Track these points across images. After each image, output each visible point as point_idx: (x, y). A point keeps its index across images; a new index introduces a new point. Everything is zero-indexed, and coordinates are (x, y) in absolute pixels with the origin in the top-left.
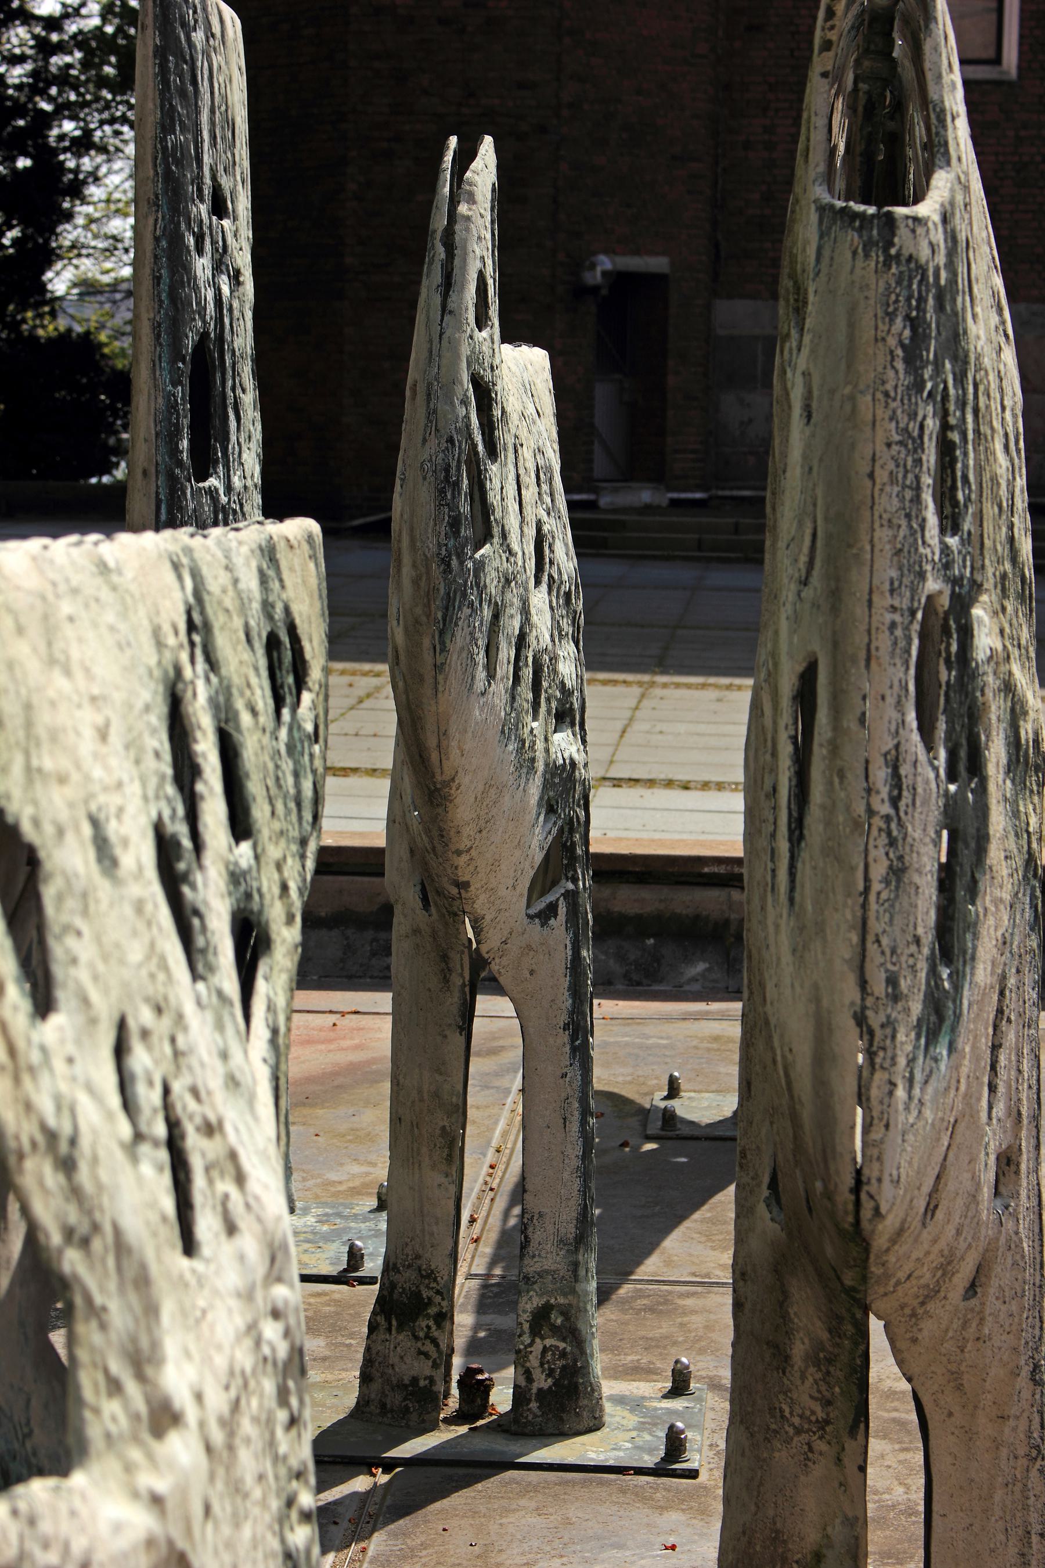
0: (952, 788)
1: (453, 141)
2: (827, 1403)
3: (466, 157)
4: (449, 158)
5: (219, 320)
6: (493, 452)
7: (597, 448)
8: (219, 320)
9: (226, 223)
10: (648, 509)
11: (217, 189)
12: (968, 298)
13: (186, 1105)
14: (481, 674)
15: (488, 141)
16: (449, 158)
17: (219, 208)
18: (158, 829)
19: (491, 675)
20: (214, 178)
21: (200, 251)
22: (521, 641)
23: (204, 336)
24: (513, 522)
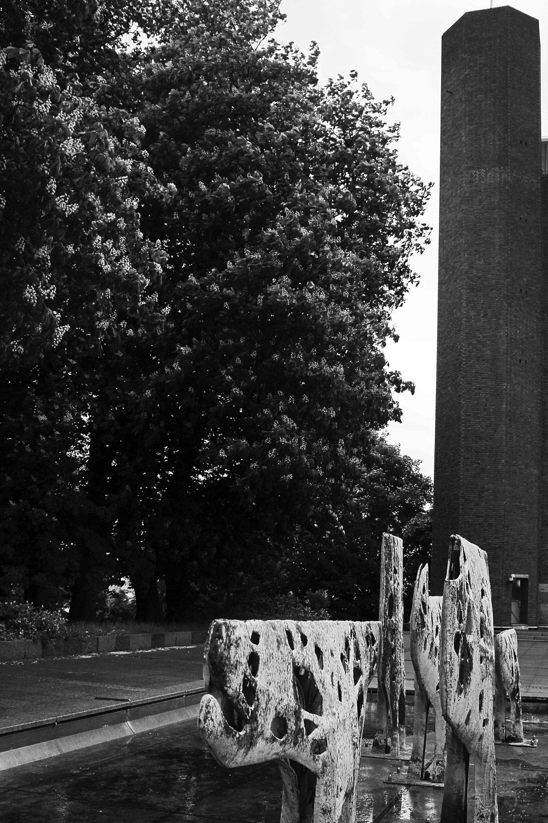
0: (463, 659)
1: (421, 564)
2: (459, 759)
3: (423, 567)
4: (420, 567)
5: (395, 592)
6: (425, 613)
7: (512, 616)
8: (395, 592)
9: (397, 575)
10: (525, 630)
11: (395, 569)
12: (466, 591)
13: (341, 683)
14: (423, 649)
15: (427, 564)
16: (420, 567)
17: (395, 572)
18: (342, 654)
19: (425, 649)
20: (394, 567)
21: (391, 579)
22: (432, 645)
23: (392, 594)
24: (430, 625)
